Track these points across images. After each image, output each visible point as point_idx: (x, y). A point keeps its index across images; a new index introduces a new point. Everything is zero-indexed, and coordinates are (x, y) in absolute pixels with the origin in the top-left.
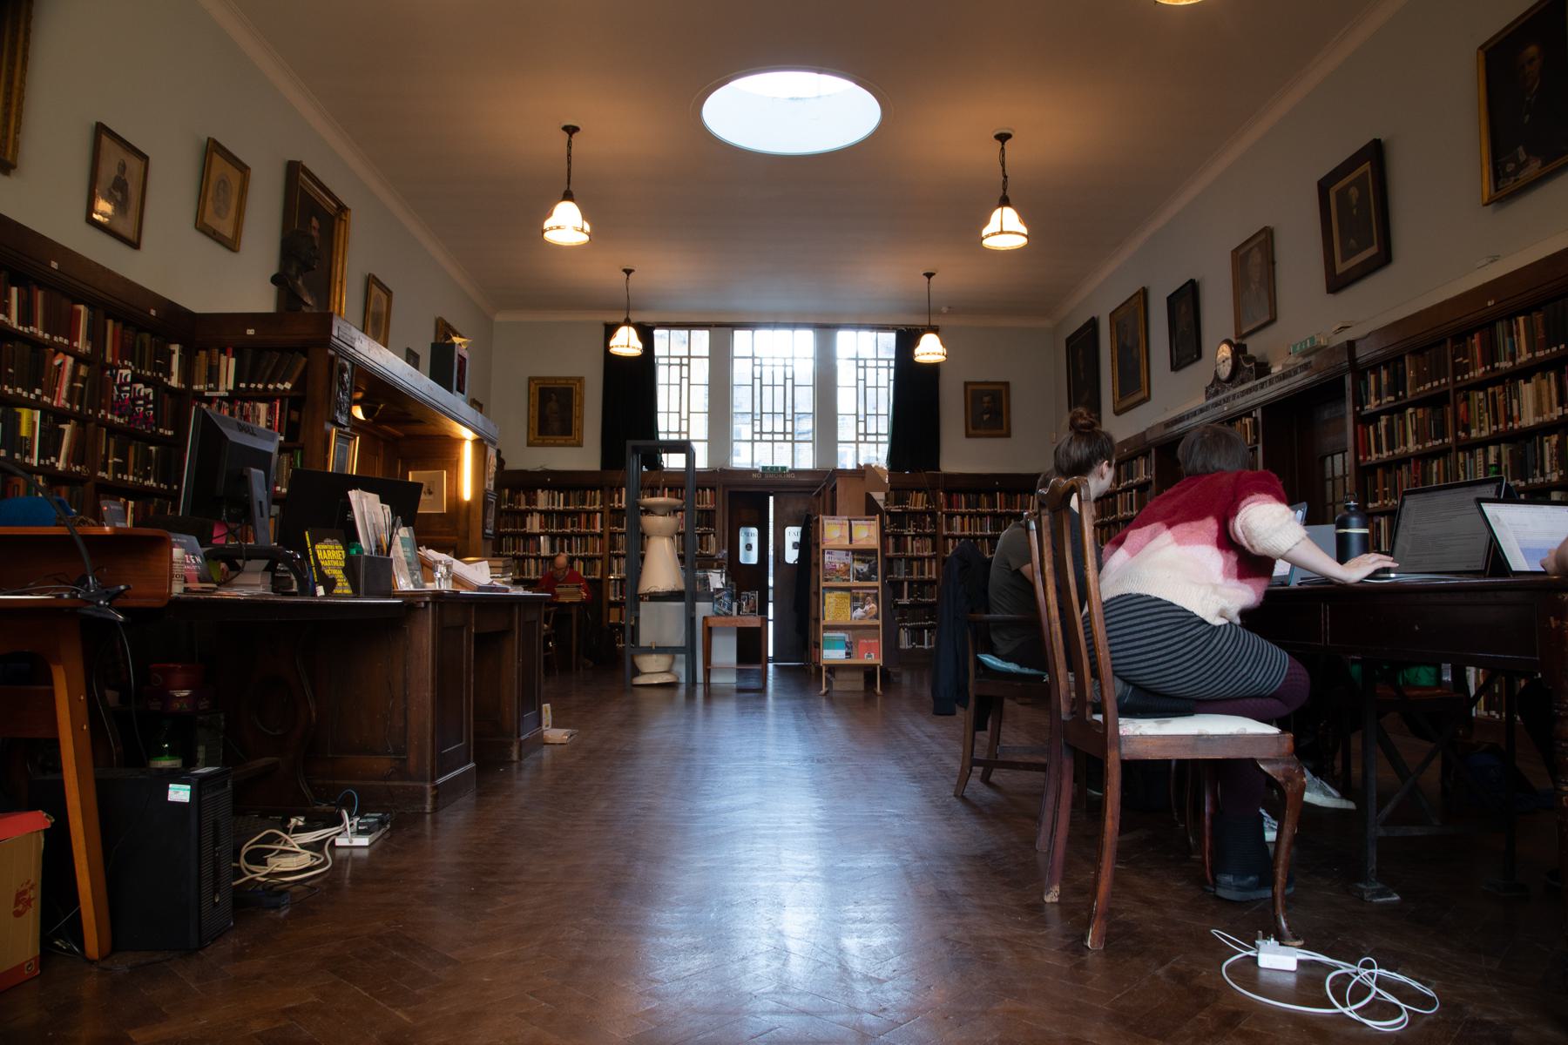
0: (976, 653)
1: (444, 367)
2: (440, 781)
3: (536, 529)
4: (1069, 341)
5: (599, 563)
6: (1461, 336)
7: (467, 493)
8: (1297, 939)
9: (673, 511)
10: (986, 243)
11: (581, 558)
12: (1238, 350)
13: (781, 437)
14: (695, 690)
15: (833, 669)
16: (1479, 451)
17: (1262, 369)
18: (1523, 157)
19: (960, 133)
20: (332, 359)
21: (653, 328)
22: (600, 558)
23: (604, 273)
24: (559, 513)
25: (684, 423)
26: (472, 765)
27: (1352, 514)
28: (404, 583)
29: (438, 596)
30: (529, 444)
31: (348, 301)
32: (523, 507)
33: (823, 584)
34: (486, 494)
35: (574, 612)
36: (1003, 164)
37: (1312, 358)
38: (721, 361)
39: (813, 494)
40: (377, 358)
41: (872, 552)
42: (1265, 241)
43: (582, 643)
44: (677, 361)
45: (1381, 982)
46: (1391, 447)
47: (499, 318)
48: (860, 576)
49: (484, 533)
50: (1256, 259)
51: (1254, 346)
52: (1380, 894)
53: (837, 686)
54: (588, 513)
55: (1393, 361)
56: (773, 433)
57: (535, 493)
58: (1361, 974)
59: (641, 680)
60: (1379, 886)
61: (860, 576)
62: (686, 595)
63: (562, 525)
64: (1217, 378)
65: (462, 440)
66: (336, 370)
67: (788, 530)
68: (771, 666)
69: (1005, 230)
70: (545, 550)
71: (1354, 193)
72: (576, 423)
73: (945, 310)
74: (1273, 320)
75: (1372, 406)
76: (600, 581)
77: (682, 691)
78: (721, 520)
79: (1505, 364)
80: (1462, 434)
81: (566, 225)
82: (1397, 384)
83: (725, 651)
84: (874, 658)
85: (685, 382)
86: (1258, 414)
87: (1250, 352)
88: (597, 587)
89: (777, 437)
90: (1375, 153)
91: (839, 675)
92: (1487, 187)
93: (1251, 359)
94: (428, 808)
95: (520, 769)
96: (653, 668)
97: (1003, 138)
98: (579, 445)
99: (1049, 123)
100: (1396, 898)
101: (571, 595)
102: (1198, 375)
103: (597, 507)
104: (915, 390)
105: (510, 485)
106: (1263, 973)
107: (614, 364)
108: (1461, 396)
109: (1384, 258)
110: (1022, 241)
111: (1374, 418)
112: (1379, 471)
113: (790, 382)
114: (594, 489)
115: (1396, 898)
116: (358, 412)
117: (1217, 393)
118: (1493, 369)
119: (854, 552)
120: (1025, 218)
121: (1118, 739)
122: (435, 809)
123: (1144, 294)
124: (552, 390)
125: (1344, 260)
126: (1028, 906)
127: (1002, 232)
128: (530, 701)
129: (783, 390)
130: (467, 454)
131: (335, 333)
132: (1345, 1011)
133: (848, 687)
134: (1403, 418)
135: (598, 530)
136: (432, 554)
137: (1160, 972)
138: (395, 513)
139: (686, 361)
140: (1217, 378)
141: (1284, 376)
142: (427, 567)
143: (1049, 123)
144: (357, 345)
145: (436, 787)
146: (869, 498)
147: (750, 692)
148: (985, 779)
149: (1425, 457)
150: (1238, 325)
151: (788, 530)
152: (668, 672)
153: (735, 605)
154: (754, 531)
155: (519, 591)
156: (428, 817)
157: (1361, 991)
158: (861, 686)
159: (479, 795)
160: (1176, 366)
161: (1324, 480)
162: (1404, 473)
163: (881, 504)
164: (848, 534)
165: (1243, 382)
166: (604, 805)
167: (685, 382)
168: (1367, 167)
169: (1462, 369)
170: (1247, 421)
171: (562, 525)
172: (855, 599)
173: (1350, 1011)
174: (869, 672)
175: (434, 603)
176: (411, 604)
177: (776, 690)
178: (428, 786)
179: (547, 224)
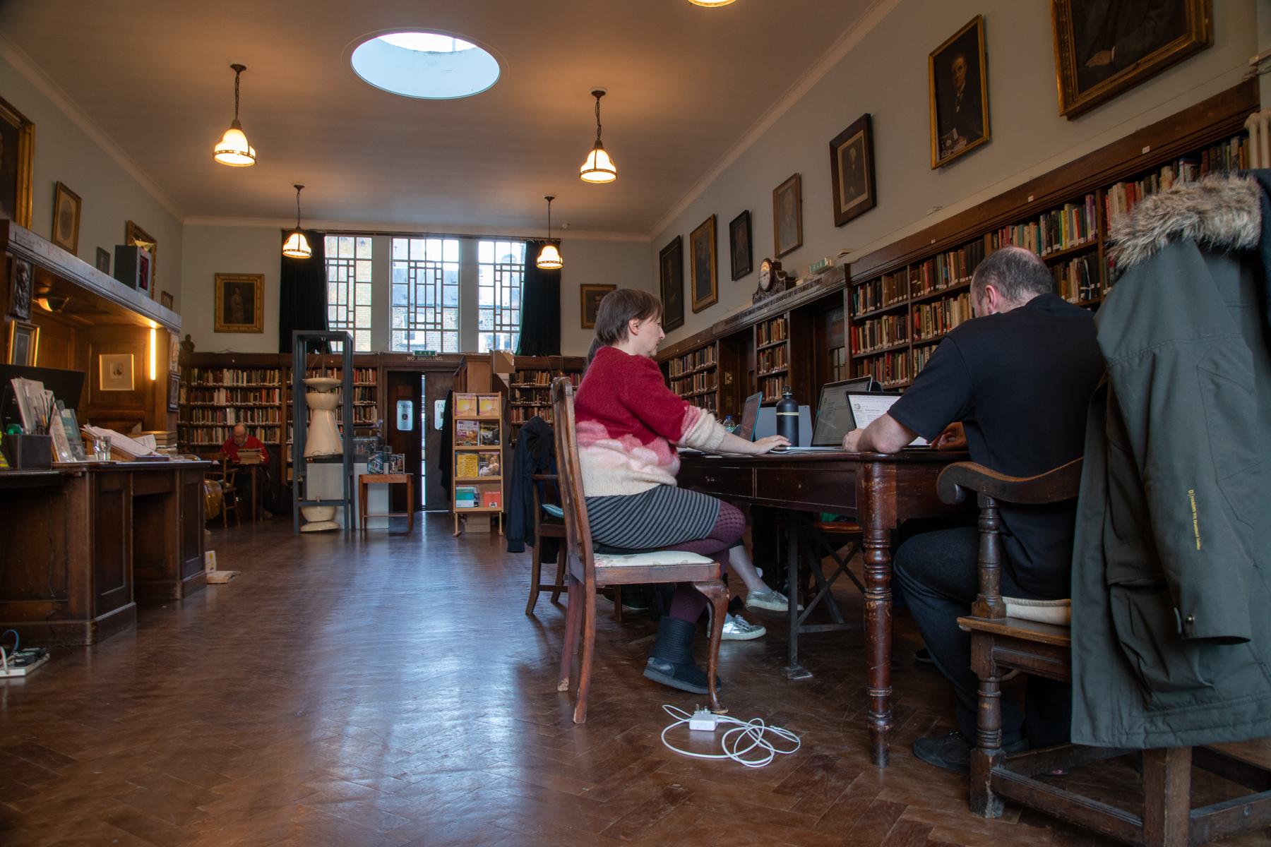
0: (541, 502)
1: (127, 266)
2: (100, 618)
3: (223, 402)
4: (662, 253)
5: (278, 431)
6: (916, 265)
7: (153, 375)
8: (723, 709)
9: (332, 389)
10: (584, 177)
11: (262, 427)
12: (775, 267)
13: (432, 327)
14: (353, 537)
15: (464, 516)
16: (926, 349)
17: (791, 282)
18: (956, 136)
19: (564, 87)
20: (10, 260)
21: (324, 235)
22: (279, 427)
23: (278, 185)
24: (242, 389)
25: (351, 315)
26: (132, 604)
27: (787, 401)
28: (65, 456)
29: (95, 469)
30: (216, 331)
31: (36, 202)
32: (211, 384)
33: (455, 448)
34: (170, 375)
35: (254, 472)
36: (598, 115)
37: (823, 276)
38: (382, 265)
39: (453, 372)
40: (57, 260)
41: (496, 422)
42: (796, 182)
43: (263, 500)
44: (345, 262)
45: (767, 735)
46: (873, 344)
47: (189, 222)
48: (485, 441)
49: (168, 407)
50: (790, 194)
51: (787, 265)
52: (799, 673)
53: (468, 529)
54: (268, 389)
55: (874, 280)
56: (425, 323)
57: (221, 372)
58: (748, 727)
59: (307, 528)
60: (799, 668)
61: (485, 441)
62: (346, 459)
63: (245, 399)
64: (760, 288)
65: (149, 328)
66: (14, 270)
67: (437, 402)
68: (424, 513)
69: (599, 167)
70: (231, 420)
71: (853, 152)
72: (257, 313)
73: (564, 226)
74: (800, 245)
75: (860, 313)
76: (279, 446)
77: (342, 536)
78: (381, 394)
79: (941, 286)
80: (916, 336)
81: (234, 149)
82: (877, 298)
83: (379, 503)
84: (497, 506)
85: (351, 280)
86: (787, 316)
87: (784, 268)
88: (275, 452)
89: (428, 327)
90: (867, 123)
91: (470, 520)
92: (935, 157)
93: (783, 274)
94: (88, 641)
95: (183, 605)
96: (318, 518)
97: (598, 94)
98: (260, 331)
99: (637, 87)
100: (810, 676)
101: (250, 458)
102: (749, 285)
103: (276, 384)
104: (541, 292)
105: (197, 367)
106: (692, 734)
107: (290, 266)
108: (915, 308)
109: (872, 203)
110: (612, 177)
111: (861, 322)
112: (865, 362)
113: (440, 279)
114: (273, 369)
115: (810, 676)
116: (45, 305)
117: (760, 299)
118: (935, 290)
119: (481, 421)
120: (614, 159)
121: (594, 571)
122: (95, 642)
123: (714, 219)
124: (237, 285)
125: (846, 203)
126: (545, 695)
127: (595, 170)
128: (193, 548)
129: (433, 287)
130: (153, 339)
131: (12, 237)
132: (732, 756)
133: (478, 529)
134: (880, 323)
135: (277, 403)
136: (95, 431)
137: (618, 737)
138: (57, 396)
139: (352, 263)
140: (760, 288)
141: (804, 288)
142: (87, 441)
143: (637, 87)
144: (36, 248)
145: (94, 624)
146: (495, 378)
147: (403, 535)
148: (554, 600)
149: (894, 352)
150: (777, 247)
151: (437, 402)
152: (331, 520)
153: (386, 465)
154: (410, 403)
155: (181, 460)
156: (88, 649)
157: (746, 742)
158: (487, 529)
159: (139, 628)
160: (736, 276)
161: (832, 368)
162: (881, 365)
163: (506, 383)
164: (477, 407)
165: (777, 291)
166: (242, 631)
167: (351, 280)
168: (861, 134)
169: (916, 289)
170: (780, 321)
171: (245, 399)
172: (482, 459)
173: (735, 756)
174: (493, 517)
175: (91, 473)
176: (68, 476)
177: (428, 530)
178: (88, 623)
179: (218, 148)
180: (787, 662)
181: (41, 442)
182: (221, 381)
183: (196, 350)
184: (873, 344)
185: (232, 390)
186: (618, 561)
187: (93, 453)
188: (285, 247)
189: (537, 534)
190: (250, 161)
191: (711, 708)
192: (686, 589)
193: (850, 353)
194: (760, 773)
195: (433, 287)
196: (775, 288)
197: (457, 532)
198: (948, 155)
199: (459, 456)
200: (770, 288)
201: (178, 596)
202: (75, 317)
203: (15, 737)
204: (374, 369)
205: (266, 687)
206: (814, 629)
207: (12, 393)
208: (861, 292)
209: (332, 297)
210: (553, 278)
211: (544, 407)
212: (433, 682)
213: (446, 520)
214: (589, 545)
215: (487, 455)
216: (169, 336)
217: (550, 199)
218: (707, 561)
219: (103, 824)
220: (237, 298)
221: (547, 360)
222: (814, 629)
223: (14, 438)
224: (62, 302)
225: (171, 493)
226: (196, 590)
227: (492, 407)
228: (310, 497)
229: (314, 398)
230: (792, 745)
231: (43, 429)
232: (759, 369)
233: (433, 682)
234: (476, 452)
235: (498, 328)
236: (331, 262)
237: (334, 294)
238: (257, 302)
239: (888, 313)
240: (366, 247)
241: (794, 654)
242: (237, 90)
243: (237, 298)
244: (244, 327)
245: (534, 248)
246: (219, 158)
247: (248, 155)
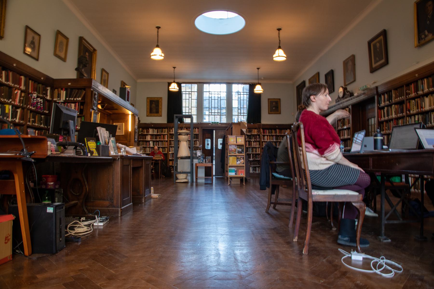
0: (272, 172)
1: (123, 94)
2: (123, 208)
3: (149, 139)
4: (297, 87)
6: (408, 85)
7: (130, 129)
9: (187, 134)
11: (161, 148)
12: (345, 89)
13: (217, 114)
14: (193, 184)
15: (231, 178)
19: (267, 28)
20: (92, 92)
22: (167, 147)
23: (168, 68)
24: (155, 135)
26: (131, 203)
28: (112, 153)
29: (122, 157)
32: (145, 133)
33: (229, 154)
34: (135, 129)
35: (160, 162)
36: (279, 37)
37: (366, 91)
38: (200, 93)
39: (227, 129)
40: (105, 91)
41: (242, 146)
42: (353, 58)
43: (163, 171)
46: (388, 116)
47: (139, 81)
48: (239, 152)
51: (349, 88)
52: (385, 239)
53: (232, 183)
54: (164, 135)
55: (388, 92)
59: (178, 181)
60: (385, 237)
61: (239, 152)
62: (191, 158)
63: (156, 138)
64: (339, 97)
65: (129, 114)
66: (93, 94)
68: (214, 177)
69: (280, 56)
71: (378, 45)
72: (160, 110)
73: (262, 78)
74: (355, 81)
75: (383, 104)
76: (167, 154)
77: (190, 184)
78: (200, 137)
79: (420, 92)
80: (408, 112)
81: (157, 54)
82: (390, 98)
83: (201, 173)
86: (350, 107)
89: (216, 114)
90: (384, 33)
92: (416, 43)
93: (348, 92)
94: (119, 215)
95: (145, 205)
96: (182, 178)
97: (279, 30)
98: (161, 116)
99: (293, 25)
100: (390, 240)
103: (166, 133)
104: (254, 101)
105: (143, 127)
109: (387, 63)
110: (285, 59)
112: (384, 123)
114: (165, 128)
115: (390, 240)
117: (339, 101)
119: (238, 145)
120: (285, 53)
121: (312, 196)
122: (121, 216)
123: (318, 74)
124: (154, 101)
125: (375, 63)
128: (147, 186)
129: (217, 100)
130: (130, 118)
131: (93, 84)
133: (236, 183)
135: (166, 140)
137: (324, 260)
139: (190, 93)
140: (339, 97)
142: (119, 149)
143: (293, 25)
144: (99, 87)
145: (121, 210)
146: (241, 131)
147: (208, 185)
148: (274, 208)
149: (397, 119)
150: (345, 82)
152: (186, 179)
153: (204, 160)
155: (145, 156)
156: (119, 218)
157: (381, 266)
158: (239, 183)
159: (133, 212)
162: (392, 124)
163: (245, 132)
164: (236, 141)
165: (346, 98)
166: (168, 214)
168: (381, 37)
169: (407, 94)
172: (238, 158)
174: (241, 179)
175: (121, 158)
176: (114, 159)
179: (152, 54)
180: (379, 234)
181: (106, 148)
182: (149, 132)
183: (141, 122)
184: (388, 116)
185: (152, 135)
186: (321, 193)
187: (120, 152)
188: (170, 88)
189: (271, 183)
190: (162, 58)
191: (358, 251)
192: (349, 205)
193: (378, 120)
194: (391, 280)
195: (217, 100)
196: (345, 97)
197: (229, 184)
198: (422, 42)
199: (230, 157)
200: (344, 97)
201: (143, 201)
202: (107, 111)
203: (106, 246)
204: (198, 128)
205: (170, 235)
206: (391, 222)
207: (97, 132)
208: (383, 97)
209: (184, 104)
210: (259, 95)
211: (255, 141)
212: (219, 234)
213: (223, 178)
214: (310, 186)
215: (239, 157)
216: (135, 117)
217: (258, 69)
218: (356, 194)
219: (144, 281)
220: (154, 105)
221: (257, 125)
222: (391, 222)
223: (99, 146)
224: (104, 106)
225: (141, 167)
226: (148, 200)
227: (241, 140)
228: (179, 170)
229: (181, 137)
230: (399, 269)
231: (107, 144)
232: (338, 127)
233: (219, 234)
234: (236, 156)
235: (239, 114)
236: (183, 93)
237: (185, 104)
238: (160, 106)
239: (396, 104)
240: (195, 87)
241: (383, 232)
242: (158, 35)
243: (154, 105)
244: (156, 114)
245: (252, 86)
246: (152, 57)
247: (162, 56)
